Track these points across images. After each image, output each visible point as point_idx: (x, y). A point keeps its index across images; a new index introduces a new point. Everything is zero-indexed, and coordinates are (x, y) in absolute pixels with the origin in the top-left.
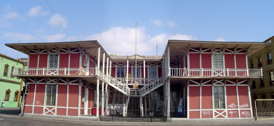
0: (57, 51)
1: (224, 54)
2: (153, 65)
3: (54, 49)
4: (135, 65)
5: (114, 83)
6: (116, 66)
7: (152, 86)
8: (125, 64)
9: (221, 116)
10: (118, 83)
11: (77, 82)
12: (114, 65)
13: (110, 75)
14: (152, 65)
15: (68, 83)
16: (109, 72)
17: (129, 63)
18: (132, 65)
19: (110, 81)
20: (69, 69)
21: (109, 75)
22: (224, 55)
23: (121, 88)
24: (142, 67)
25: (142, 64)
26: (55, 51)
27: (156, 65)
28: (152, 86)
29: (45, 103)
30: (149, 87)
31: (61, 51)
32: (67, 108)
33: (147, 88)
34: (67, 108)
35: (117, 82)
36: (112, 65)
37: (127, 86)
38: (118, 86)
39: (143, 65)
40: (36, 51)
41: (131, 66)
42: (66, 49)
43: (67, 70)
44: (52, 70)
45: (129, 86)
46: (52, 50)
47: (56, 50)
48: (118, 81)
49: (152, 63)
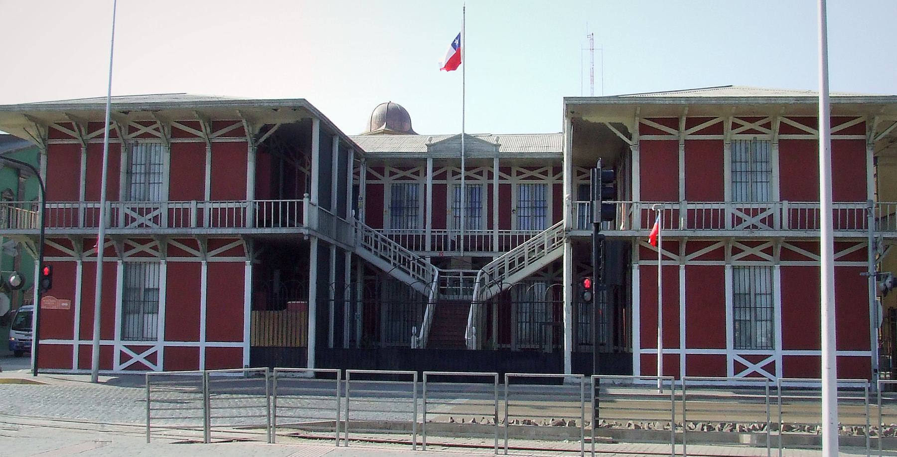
0: (157, 130)
1: (776, 141)
2: (535, 173)
3: (147, 124)
4: (458, 177)
5: (414, 270)
6: (387, 182)
7: (521, 259)
8: (422, 174)
9: (755, 359)
10: (392, 248)
11: (238, 251)
12: (378, 176)
13: (360, 216)
14: (529, 173)
15: (205, 258)
16: (355, 207)
17: (434, 170)
18: (449, 175)
19: (361, 240)
20: (208, 206)
21: (356, 217)
22: (776, 146)
23: (406, 268)
24: (490, 182)
25: (490, 169)
26: (149, 130)
27: (545, 173)
28: (521, 259)
29: (461, 289)
30: (511, 265)
31: (176, 133)
32: (202, 344)
33: (534, 251)
34: (202, 344)
35: (422, 267)
36: (369, 176)
37: (428, 261)
38: (392, 259)
39: (491, 176)
40: (73, 130)
41: (445, 179)
42: (196, 125)
43: (200, 206)
44: (141, 210)
45: (436, 261)
46: (139, 126)
47: (155, 126)
48: (393, 242)
49: (531, 169)
